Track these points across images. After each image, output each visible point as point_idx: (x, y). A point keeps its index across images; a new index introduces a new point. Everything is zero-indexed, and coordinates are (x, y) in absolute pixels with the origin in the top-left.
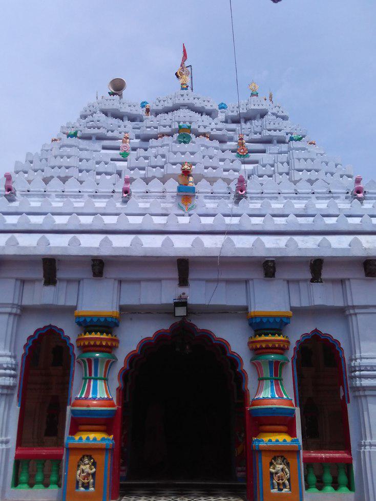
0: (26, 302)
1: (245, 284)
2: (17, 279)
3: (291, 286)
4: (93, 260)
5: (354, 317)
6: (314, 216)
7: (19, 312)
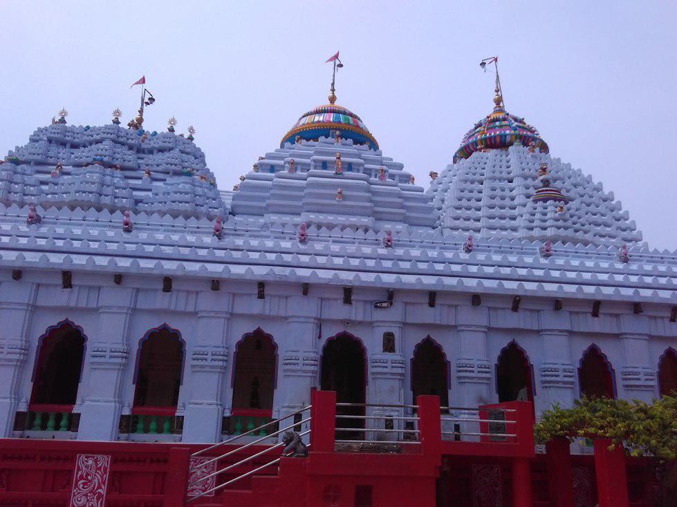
0: (493, 325)
2: (319, 298)
3: (491, 312)
4: (165, 277)
5: (625, 340)
7: (228, 316)
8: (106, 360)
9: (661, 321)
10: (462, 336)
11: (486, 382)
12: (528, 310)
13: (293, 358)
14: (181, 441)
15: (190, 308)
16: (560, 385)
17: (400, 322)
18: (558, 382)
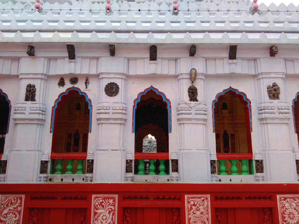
1: (253, 61)
3: (288, 63)
6: (283, 23)
7: (46, 78)
8: (277, 115)
9: (291, 63)
10: (181, 82)
11: (202, 122)
12: (87, 58)
13: (38, 109)
14: (91, 181)
15: (172, 73)
16: (276, 121)
17: (123, 74)
18: (190, 119)
